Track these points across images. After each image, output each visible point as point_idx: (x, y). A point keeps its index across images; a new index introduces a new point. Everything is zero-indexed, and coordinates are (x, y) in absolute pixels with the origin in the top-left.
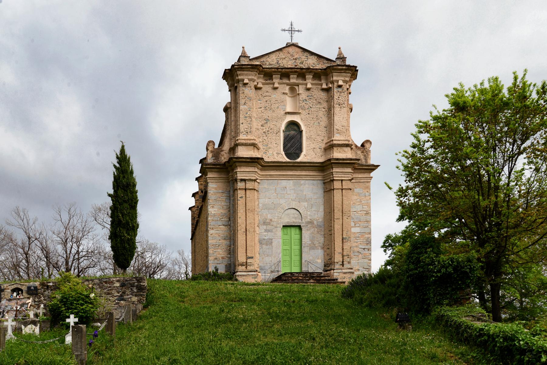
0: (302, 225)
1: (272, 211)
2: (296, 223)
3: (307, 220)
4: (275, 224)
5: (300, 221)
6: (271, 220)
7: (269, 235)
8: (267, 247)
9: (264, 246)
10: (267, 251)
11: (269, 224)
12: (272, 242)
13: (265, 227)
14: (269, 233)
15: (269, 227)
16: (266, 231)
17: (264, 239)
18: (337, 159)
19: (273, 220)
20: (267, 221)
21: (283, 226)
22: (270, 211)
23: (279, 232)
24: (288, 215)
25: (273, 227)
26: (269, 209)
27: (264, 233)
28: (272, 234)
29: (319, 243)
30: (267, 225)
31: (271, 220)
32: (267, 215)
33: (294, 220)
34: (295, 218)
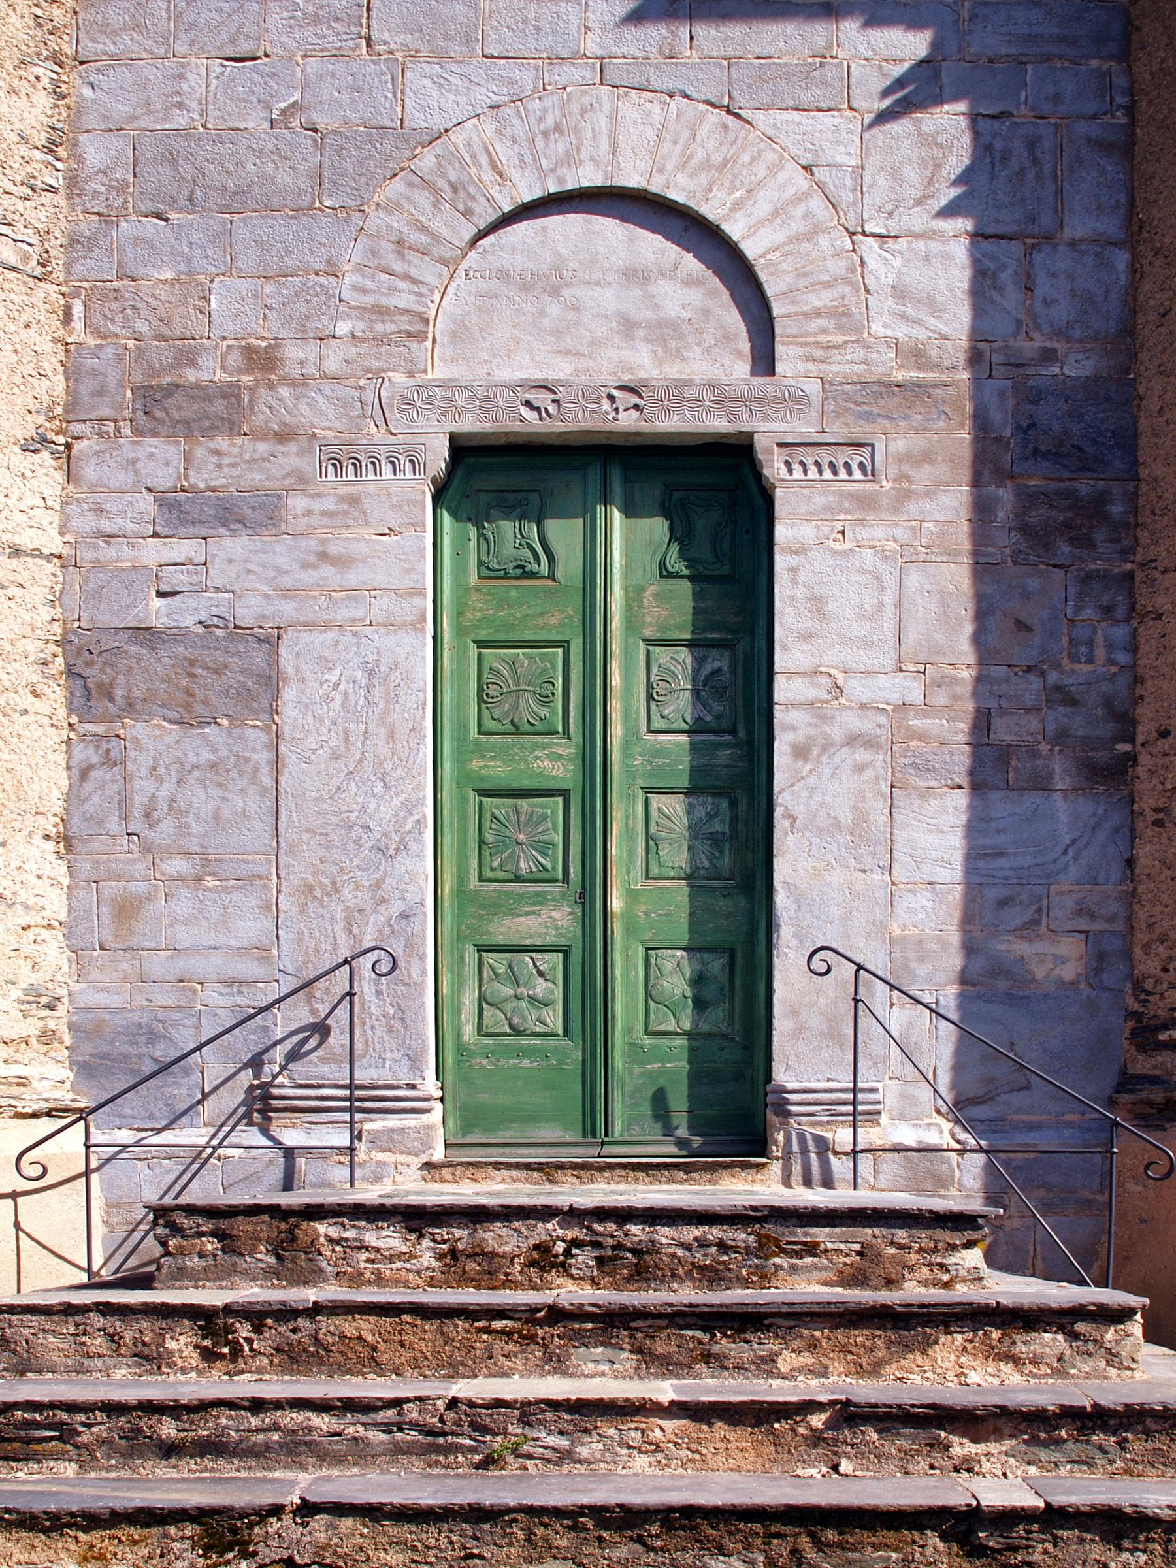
0: (767, 432)
1: (284, 229)
2: (676, 394)
3: (847, 365)
4: (322, 414)
5: (737, 369)
6: (262, 360)
7: (237, 575)
8: (200, 746)
9: (150, 737)
10: (200, 798)
11: (218, 413)
12: (272, 681)
13: (161, 460)
14: (233, 546)
15: (224, 464)
16: (179, 510)
17: (143, 633)
18: (482, 806)
19: (293, 352)
20: (209, 371)
21: (462, 450)
22: (248, 229)
23: (397, 549)
24: (550, 283)
25: (290, 458)
26: (236, 202)
27: (153, 553)
28: (281, 553)
29: (1062, 696)
30: (188, 429)
31: (262, 360)
32: (192, 288)
33: (644, 363)
34: (667, 334)
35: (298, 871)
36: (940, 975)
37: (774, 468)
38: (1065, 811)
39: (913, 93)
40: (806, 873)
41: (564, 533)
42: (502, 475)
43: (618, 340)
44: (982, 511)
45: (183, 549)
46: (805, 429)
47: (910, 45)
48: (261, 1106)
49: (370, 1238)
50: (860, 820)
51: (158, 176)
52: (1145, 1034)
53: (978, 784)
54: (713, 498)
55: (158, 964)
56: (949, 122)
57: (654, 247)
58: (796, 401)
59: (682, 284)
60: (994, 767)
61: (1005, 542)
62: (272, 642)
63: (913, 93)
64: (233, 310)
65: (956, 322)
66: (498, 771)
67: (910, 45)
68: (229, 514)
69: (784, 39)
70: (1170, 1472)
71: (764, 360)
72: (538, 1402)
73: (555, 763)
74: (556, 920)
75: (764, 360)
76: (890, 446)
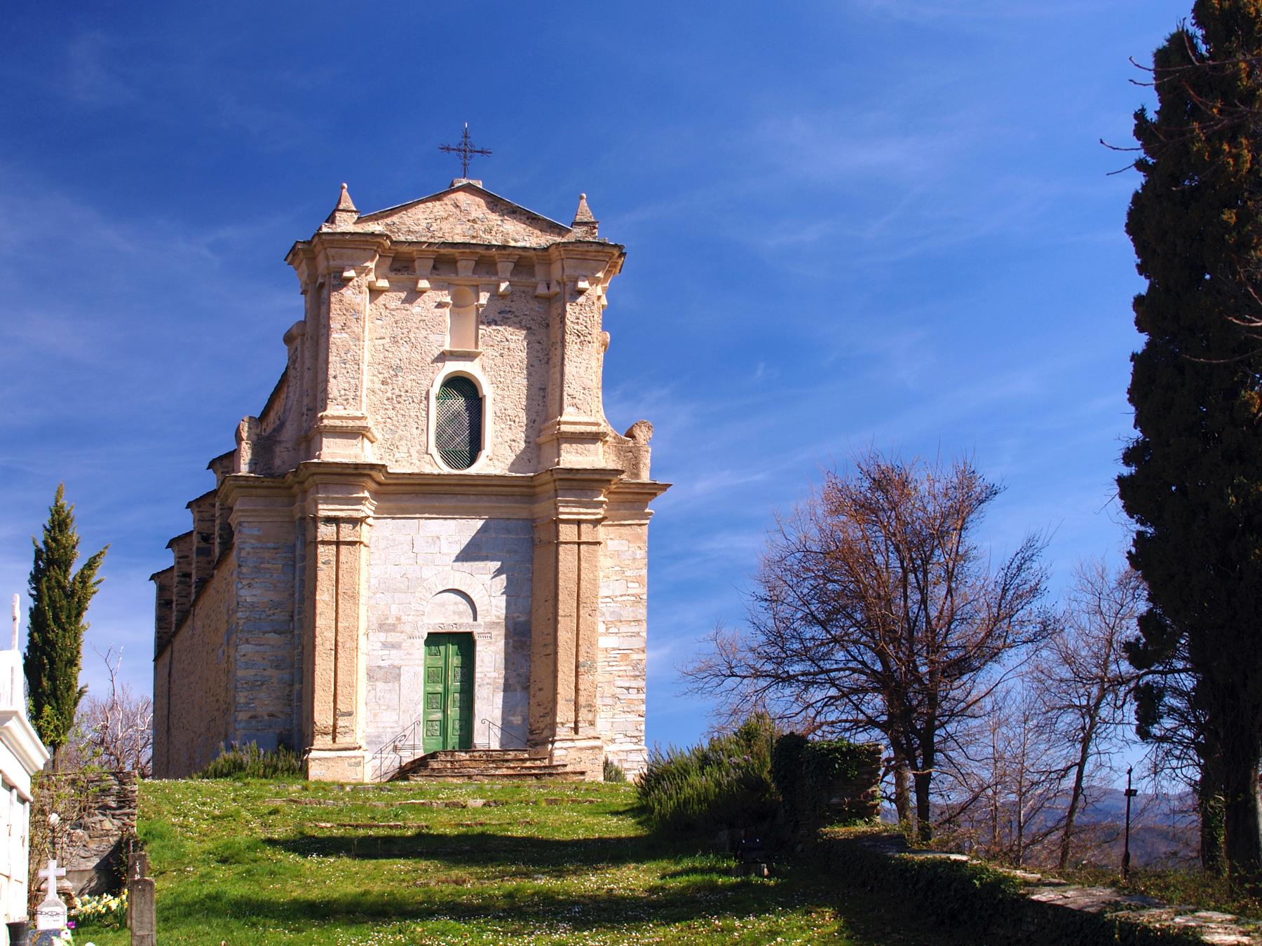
0: (476, 631)
2: (461, 625)
3: (488, 619)
4: (408, 628)
5: (471, 620)
9: (380, 685)
10: (387, 696)
11: (392, 628)
12: (399, 675)
13: (382, 636)
14: (394, 652)
15: (393, 637)
16: (385, 645)
20: (390, 621)
23: (418, 650)
24: (443, 605)
25: (403, 636)
26: (395, 591)
27: (381, 653)
28: (401, 653)
29: (519, 675)
30: (387, 631)
31: (399, 619)
35: (403, 708)
36: (499, 723)
37: (476, 638)
38: (519, 694)
39: (498, 572)
40: (479, 706)
41: (442, 648)
42: (435, 640)
43: (453, 617)
44: (507, 644)
45: (386, 652)
46: (481, 630)
47: (498, 564)
48: (395, 749)
49: (307, 344)
50: (488, 699)
51: (382, 586)
52: (531, 732)
53: (505, 691)
54: (465, 643)
55: (380, 725)
56: (504, 576)
57: (458, 599)
58: (480, 625)
59: (463, 605)
60: (507, 688)
61: (511, 650)
62: (399, 668)
63: (498, 572)
64: (395, 610)
65: (502, 612)
66: (430, 690)
67: (498, 564)
68: (393, 646)
69: (480, 564)
70: (1252, 904)
71: (475, 619)
72: (333, 783)
73: (440, 688)
74: (439, 716)
75: (475, 619)
76: (494, 633)
